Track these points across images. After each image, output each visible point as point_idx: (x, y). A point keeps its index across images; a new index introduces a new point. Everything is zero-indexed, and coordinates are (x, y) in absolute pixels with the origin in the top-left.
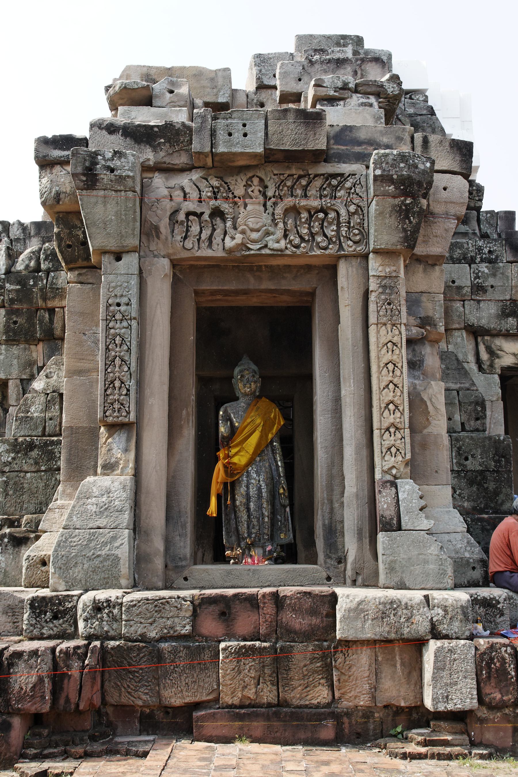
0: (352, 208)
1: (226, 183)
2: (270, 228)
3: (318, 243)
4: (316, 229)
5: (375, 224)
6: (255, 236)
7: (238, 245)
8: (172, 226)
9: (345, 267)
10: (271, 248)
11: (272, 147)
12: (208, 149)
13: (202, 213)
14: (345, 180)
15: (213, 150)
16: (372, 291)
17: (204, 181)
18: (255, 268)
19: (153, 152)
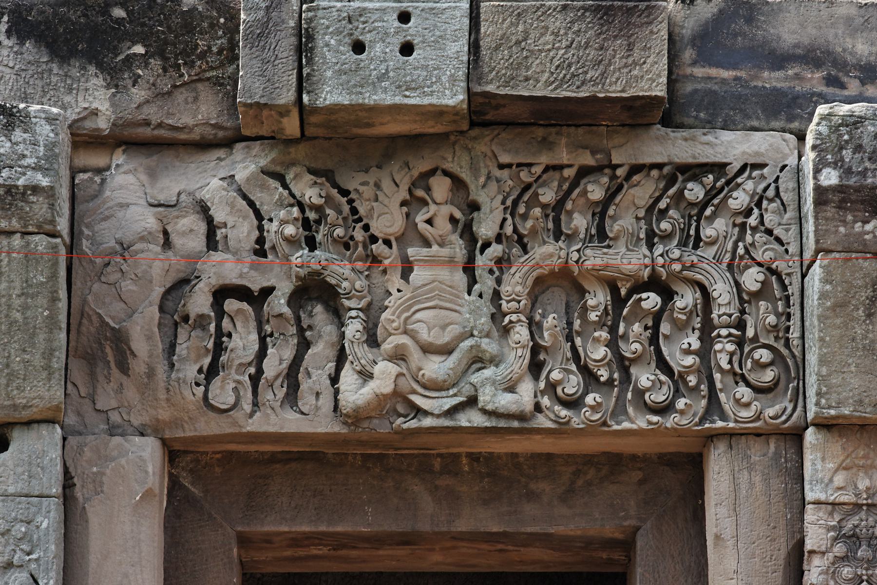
0: (752, 279)
1: (345, 193)
2: (485, 343)
3: (640, 393)
4: (632, 348)
5: (821, 339)
6: (436, 368)
7: (381, 399)
8: (170, 332)
9: (726, 470)
10: (489, 407)
11: (491, 88)
12: (287, 96)
13: (268, 291)
14: (728, 183)
15: (306, 98)
16: (812, 552)
17: (274, 184)
18: (437, 464)
19: (108, 87)
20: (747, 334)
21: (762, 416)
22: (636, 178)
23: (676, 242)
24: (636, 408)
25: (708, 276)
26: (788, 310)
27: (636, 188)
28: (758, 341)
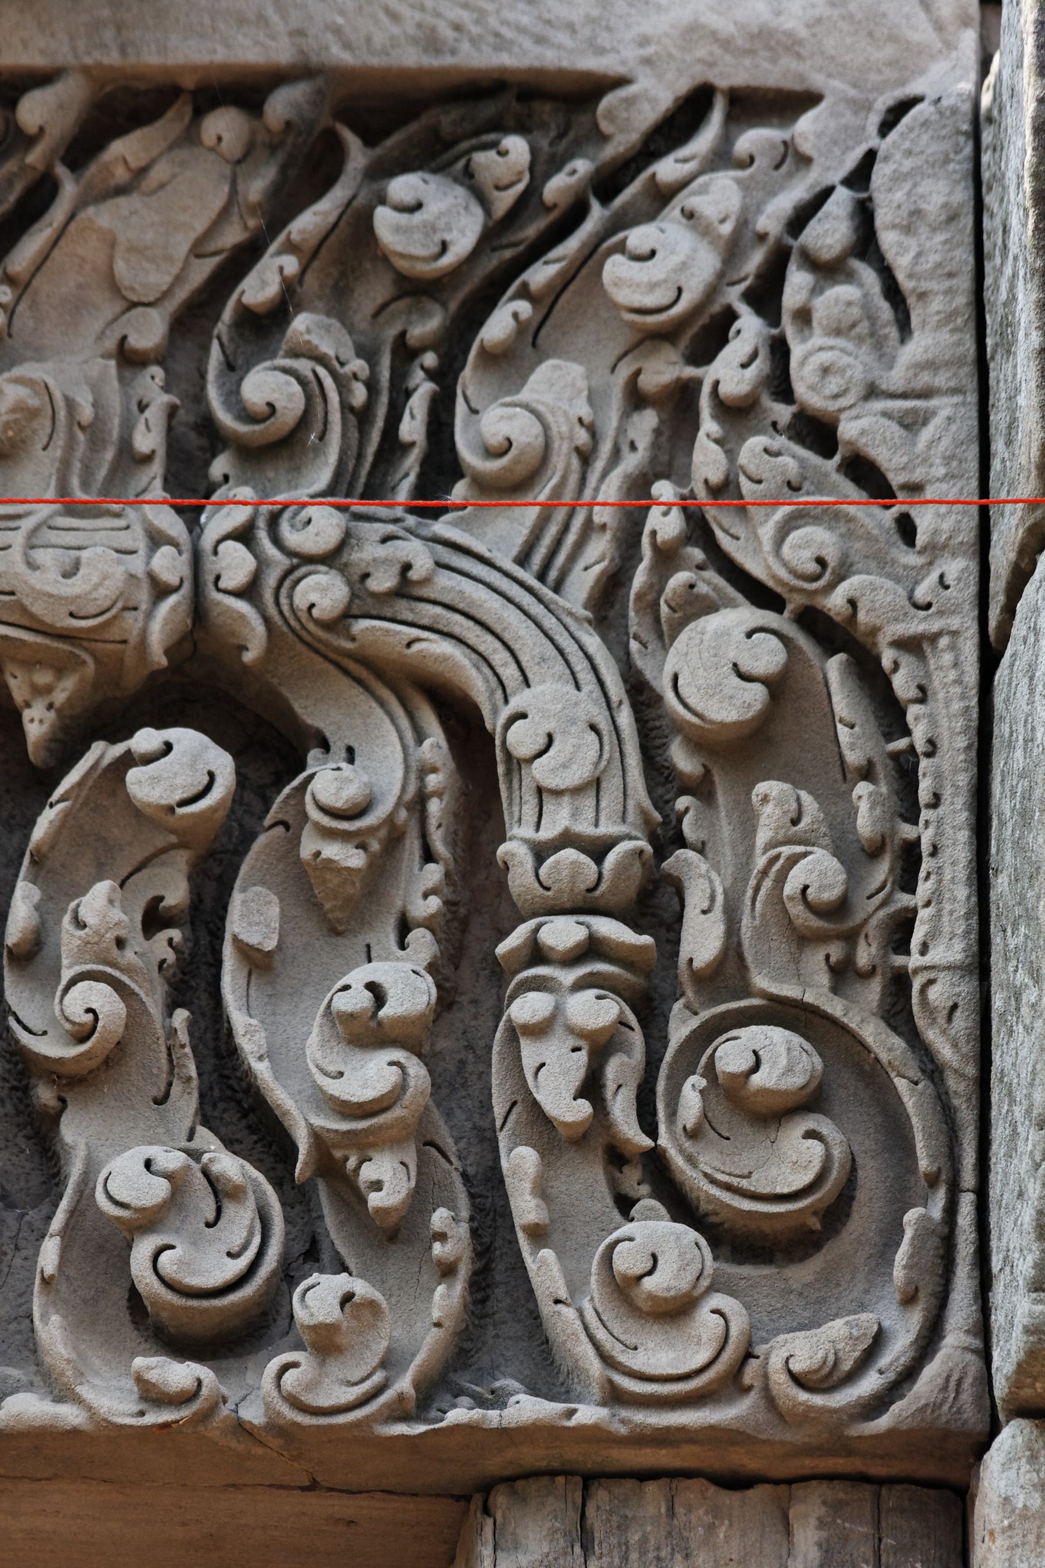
0: (716, 663)
3: (105, 1242)
14: (607, 184)
20: (686, 950)
21: (751, 1373)
22: (124, 150)
23: (323, 477)
24: (85, 1321)
25: (487, 644)
26: (908, 831)
27: (122, 202)
28: (745, 990)
